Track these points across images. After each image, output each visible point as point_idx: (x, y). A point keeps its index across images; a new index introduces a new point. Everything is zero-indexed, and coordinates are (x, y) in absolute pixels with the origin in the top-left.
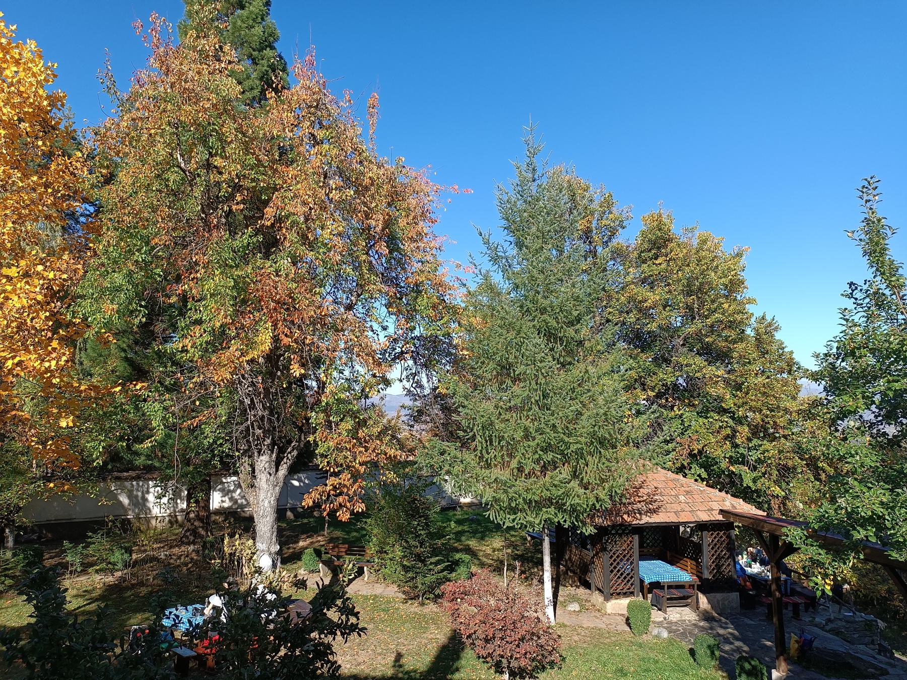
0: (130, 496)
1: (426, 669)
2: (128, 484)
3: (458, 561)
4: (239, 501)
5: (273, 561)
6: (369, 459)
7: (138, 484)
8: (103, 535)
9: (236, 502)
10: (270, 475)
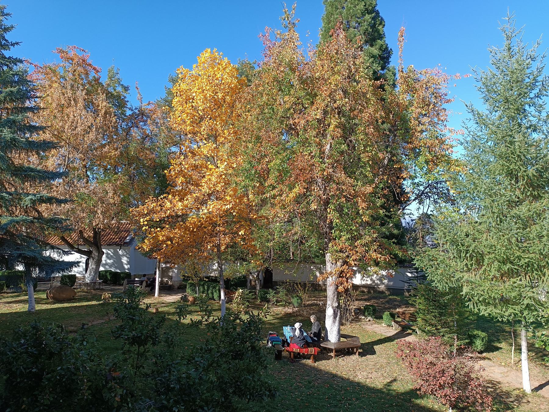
1: (403, 392)
3: (475, 335)
4: (376, 282)
5: (334, 311)
6: (64, 198)
9: (374, 282)
10: (333, 264)
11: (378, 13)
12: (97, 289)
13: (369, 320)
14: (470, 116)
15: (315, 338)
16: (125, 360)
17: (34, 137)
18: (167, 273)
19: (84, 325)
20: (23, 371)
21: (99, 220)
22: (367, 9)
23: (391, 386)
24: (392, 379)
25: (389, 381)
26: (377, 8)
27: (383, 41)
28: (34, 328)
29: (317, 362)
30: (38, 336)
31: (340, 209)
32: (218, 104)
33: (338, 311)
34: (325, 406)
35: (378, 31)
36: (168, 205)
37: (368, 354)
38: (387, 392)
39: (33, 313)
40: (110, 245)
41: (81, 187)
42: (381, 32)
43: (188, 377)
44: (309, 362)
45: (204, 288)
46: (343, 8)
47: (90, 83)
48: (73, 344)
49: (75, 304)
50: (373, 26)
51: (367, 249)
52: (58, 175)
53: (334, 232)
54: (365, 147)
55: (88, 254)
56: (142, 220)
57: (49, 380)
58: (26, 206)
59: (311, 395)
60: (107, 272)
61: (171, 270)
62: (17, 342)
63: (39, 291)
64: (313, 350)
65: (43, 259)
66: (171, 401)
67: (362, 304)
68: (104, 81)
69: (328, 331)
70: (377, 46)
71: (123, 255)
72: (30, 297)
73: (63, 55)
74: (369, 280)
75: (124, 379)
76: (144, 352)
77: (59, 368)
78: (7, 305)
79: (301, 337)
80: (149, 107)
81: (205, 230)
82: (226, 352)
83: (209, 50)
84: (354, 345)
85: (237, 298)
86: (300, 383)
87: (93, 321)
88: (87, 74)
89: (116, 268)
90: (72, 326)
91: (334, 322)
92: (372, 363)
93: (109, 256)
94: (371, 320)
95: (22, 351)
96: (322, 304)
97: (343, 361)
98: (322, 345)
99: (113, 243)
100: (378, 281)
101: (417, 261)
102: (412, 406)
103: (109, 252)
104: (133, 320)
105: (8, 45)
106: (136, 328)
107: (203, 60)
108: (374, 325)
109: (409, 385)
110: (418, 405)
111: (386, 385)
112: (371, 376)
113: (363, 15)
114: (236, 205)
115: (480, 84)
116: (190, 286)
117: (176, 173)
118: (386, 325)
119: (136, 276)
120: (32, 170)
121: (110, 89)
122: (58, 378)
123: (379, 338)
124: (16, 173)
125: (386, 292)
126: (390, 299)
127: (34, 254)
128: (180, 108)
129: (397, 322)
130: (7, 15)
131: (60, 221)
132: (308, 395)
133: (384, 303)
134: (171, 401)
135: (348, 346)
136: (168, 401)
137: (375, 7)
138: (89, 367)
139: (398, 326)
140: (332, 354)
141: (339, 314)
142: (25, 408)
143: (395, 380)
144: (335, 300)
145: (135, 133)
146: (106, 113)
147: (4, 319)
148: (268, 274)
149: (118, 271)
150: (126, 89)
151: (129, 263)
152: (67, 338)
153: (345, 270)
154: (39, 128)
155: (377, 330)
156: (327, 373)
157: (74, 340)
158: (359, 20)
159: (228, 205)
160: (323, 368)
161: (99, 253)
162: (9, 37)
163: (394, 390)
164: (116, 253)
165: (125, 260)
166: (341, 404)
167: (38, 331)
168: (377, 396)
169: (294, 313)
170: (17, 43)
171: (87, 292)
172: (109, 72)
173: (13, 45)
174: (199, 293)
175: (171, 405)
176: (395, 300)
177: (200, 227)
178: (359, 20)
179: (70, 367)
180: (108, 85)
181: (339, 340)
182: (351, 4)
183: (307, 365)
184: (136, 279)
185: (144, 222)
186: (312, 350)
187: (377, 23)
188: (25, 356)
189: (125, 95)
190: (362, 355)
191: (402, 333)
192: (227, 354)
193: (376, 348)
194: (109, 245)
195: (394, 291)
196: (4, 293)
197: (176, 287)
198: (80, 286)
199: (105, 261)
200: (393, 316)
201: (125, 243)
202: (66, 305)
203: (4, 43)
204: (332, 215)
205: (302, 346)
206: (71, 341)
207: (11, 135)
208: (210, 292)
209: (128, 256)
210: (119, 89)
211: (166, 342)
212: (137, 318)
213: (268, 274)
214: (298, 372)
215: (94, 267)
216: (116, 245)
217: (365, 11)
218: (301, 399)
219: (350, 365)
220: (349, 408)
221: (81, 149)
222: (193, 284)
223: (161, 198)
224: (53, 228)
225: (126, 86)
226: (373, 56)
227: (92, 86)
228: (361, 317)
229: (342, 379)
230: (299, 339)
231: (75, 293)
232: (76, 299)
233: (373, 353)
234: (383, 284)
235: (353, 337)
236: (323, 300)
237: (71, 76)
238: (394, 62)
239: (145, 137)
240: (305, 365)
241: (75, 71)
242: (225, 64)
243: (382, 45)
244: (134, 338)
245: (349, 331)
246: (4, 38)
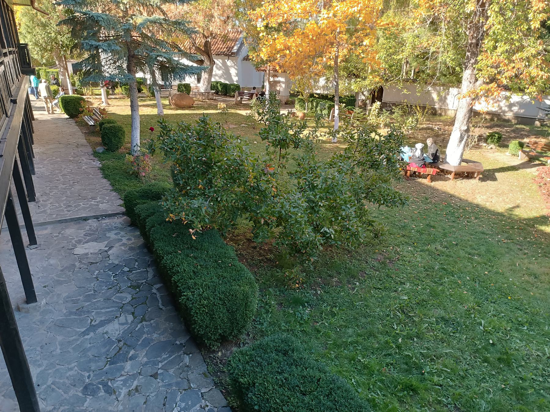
0: (439, 95)
2: (438, 88)
4: (503, 108)
5: (461, 134)
7: (443, 88)
8: (399, 109)
9: (501, 108)
10: (470, 83)
13: (491, 148)
18: (275, 88)
23: (513, 211)
24: (515, 205)
25: (511, 206)
29: (433, 182)
33: (465, 135)
34: (443, 220)
37: (488, 179)
38: (509, 216)
40: (219, 55)
44: (426, 181)
45: (312, 104)
59: (429, 210)
60: (218, 83)
61: (278, 85)
64: (432, 170)
66: (318, 197)
67: (487, 132)
71: (232, 66)
76: (286, 154)
79: (420, 157)
81: (327, 37)
85: (374, 110)
86: (417, 198)
89: (225, 79)
93: (218, 66)
96: (438, 128)
98: (440, 167)
99: (221, 53)
102: (536, 231)
108: (497, 154)
109: (533, 212)
110: (541, 231)
111: (507, 210)
112: (491, 200)
116: (299, 102)
123: (501, 166)
125: (513, 121)
126: (517, 129)
129: (524, 152)
132: (425, 209)
133: (508, 132)
134: (318, 197)
136: (315, 196)
139: (524, 156)
140: (451, 176)
142: (201, 188)
143: (518, 206)
144: (465, 122)
149: (227, 82)
151: (237, 75)
153: (492, 89)
156: (444, 193)
159: (356, 7)
160: (439, 188)
161: (210, 63)
163: (517, 215)
164: (224, 64)
166: (459, 220)
168: (498, 218)
171: (203, 102)
174: (308, 109)
175: (317, 199)
176: (523, 130)
177: (319, 35)
181: (460, 164)
183: (423, 184)
184: (246, 91)
186: (430, 171)
190: (482, 180)
191: (528, 164)
192: (365, 163)
193: (497, 175)
195: (522, 120)
197: (284, 102)
200: (521, 145)
205: (421, 166)
208: (318, 108)
209: (236, 67)
215: (207, 77)
216: (224, 55)
218: (419, 212)
220: (467, 225)
222: (302, 99)
228: (482, 144)
229: (460, 199)
230: (418, 159)
232: (195, 107)
233: (494, 179)
234: (512, 111)
235: (474, 162)
236: (439, 125)
240: (420, 184)
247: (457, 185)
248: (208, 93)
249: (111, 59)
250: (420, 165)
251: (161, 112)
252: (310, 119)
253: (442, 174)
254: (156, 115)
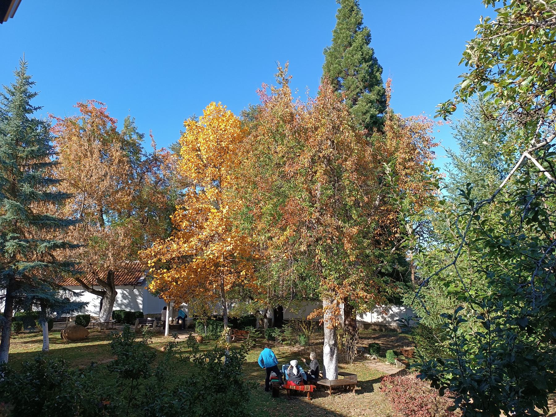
4: (387, 319)
5: (331, 349)
9: (385, 319)
11: (376, 60)
12: (110, 329)
13: (374, 359)
14: (450, 160)
15: (313, 376)
16: (119, 393)
17: (53, 189)
19: (93, 363)
20: (28, 400)
21: (110, 262)
22: (364, 58)
26: (375, 56)
27: (380, 87)
28: (37, 362)
30: (40, 368)
31: (327, 250)
32: (223, 151)
33: (334, 349)
35: (375, 77)
36: (175, 246)
39: (47, 352)
41: (96, 231)
42: (378, 78)
43: (171, 406)
46: (342, 57)
47: (107, 133)
48: (71, 376)
49: (87, 344)
50: (371, 74)
51: (354, 287)
52: (73, 222)
53: (325, 271)
54: (350, 191)
55: (102, 294)
56: (149, 262)
57: (48, 407)
58: (41, 252)
62: (24, 375)
63: (55, 331)
64: (309, 387)
65: (55, 301)
68: (121, 129)
69: (326, 368)
70: (375, 92)
72: (45, 338)
73: (82, 108)
74: (381, 318)
75: (115, 408)
77: (58, 397)
78: (24, 345)
80: (162, 153)
82: (210, 386)
83: (214, 104)
84: (350, 382)
87: (103, 360)
88: (104, 124)
89: (132, 308)
90: (82, 365)
91: (331, 360)
92: (368, 401)
94: (376, 358)
95: (27, 382)
97: (339, 399)
99: (130, 283)
100: (389, 319)
101: (406, 298)
103: (125, 292)
104: (126, 355)
105: (31, 110)
106: (129, 363)
107: (208, 113)
112: (364, 413)
113: (360, 63)
114: (236, 246)
115: (456, 132)
117: (180, 218)
118: (389, 363)
119: (149, 316)
120: (47, 218)
121: (127, 138)
122: (56, 405)
124: (33, 222)
125: (398, 330)
127: (46, 296)
128: (186, 157)
129: (400, 360)
130: (32, 83)
131: (72, 264)
135: (345, 384)
137: (372, 56)
138: (83, 396)
139: (401, 363)
140: (329, 392)
141: (336, 352)
144: (332, 337)
145: (150, 178)
146: (120, 161)
147: (19, 358)
148: (278, 313)
149: (133, 311)
150: (141, 136)
152: (66, 372)
154: (55, 181)
155: (380, 368)
157: (73, 373)
158: (357, 69)
159: (229, 247)
161: (112, 294)
162: (33, 102)
164: (131, 293)
165: (140, 300)
167: (41, 364)
169: (299, 352)
170: (39, 108)
171: (100, 332)
172: (126, 121)
173: (36, 109)
176: (405, 338)
178: (357, 69)
179: (66, 395)
180: (125, 133)
181: (337, 378)
182: (349, 54)
184: (149, 319)
185: (151, 263)
186: (308, 388)
187: (375, 70)
188: (29, 386)
189: (140, 142)
190: (358, 392)
194: (125, 285)
196: (22, 333)
198: (94, 326)
199: (121, 301)
200: (396, 353)
201: (138, 283)
202: (79, 344)
203: (28, 108)
204: (320, 255)
205: (299, 383)
206: (70, 374)
207: (31, 189)
210: (134, 137)
211: (156, 375)
212: (130, 354)
213: (278, 313)
214: (293, 409)
217: (362, 59)
219: (345, 402)
221: (96, 196)
223: (168, 241)
224: (65, 272)
225: (141, 134)
226: (371, 102)
227: (109, 135)
228: (366, 355)
231: (89, 333)
233: (371, 390)
237: (89, 126)
238: (391, 105)
239: (158, 181)
241: (93, 122)
242: (228, 116)
243: (380, 91)
244: (126, 371)
245: (352, 369)
246: (28, 104)
247: (335, 400)
248: (107, 323)
249: (301, 197)
250: (298, 382)
251: (46, 348)
252: (208, 342)
253: (320, 391)
254: (40, 351)
